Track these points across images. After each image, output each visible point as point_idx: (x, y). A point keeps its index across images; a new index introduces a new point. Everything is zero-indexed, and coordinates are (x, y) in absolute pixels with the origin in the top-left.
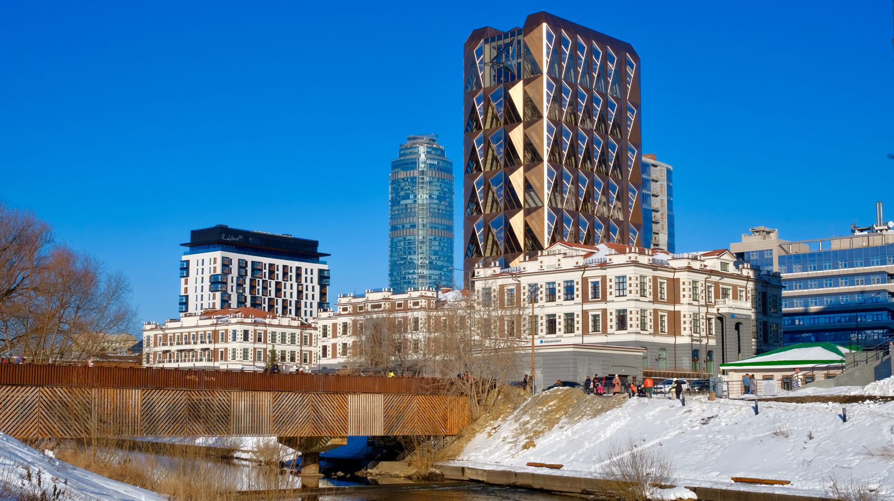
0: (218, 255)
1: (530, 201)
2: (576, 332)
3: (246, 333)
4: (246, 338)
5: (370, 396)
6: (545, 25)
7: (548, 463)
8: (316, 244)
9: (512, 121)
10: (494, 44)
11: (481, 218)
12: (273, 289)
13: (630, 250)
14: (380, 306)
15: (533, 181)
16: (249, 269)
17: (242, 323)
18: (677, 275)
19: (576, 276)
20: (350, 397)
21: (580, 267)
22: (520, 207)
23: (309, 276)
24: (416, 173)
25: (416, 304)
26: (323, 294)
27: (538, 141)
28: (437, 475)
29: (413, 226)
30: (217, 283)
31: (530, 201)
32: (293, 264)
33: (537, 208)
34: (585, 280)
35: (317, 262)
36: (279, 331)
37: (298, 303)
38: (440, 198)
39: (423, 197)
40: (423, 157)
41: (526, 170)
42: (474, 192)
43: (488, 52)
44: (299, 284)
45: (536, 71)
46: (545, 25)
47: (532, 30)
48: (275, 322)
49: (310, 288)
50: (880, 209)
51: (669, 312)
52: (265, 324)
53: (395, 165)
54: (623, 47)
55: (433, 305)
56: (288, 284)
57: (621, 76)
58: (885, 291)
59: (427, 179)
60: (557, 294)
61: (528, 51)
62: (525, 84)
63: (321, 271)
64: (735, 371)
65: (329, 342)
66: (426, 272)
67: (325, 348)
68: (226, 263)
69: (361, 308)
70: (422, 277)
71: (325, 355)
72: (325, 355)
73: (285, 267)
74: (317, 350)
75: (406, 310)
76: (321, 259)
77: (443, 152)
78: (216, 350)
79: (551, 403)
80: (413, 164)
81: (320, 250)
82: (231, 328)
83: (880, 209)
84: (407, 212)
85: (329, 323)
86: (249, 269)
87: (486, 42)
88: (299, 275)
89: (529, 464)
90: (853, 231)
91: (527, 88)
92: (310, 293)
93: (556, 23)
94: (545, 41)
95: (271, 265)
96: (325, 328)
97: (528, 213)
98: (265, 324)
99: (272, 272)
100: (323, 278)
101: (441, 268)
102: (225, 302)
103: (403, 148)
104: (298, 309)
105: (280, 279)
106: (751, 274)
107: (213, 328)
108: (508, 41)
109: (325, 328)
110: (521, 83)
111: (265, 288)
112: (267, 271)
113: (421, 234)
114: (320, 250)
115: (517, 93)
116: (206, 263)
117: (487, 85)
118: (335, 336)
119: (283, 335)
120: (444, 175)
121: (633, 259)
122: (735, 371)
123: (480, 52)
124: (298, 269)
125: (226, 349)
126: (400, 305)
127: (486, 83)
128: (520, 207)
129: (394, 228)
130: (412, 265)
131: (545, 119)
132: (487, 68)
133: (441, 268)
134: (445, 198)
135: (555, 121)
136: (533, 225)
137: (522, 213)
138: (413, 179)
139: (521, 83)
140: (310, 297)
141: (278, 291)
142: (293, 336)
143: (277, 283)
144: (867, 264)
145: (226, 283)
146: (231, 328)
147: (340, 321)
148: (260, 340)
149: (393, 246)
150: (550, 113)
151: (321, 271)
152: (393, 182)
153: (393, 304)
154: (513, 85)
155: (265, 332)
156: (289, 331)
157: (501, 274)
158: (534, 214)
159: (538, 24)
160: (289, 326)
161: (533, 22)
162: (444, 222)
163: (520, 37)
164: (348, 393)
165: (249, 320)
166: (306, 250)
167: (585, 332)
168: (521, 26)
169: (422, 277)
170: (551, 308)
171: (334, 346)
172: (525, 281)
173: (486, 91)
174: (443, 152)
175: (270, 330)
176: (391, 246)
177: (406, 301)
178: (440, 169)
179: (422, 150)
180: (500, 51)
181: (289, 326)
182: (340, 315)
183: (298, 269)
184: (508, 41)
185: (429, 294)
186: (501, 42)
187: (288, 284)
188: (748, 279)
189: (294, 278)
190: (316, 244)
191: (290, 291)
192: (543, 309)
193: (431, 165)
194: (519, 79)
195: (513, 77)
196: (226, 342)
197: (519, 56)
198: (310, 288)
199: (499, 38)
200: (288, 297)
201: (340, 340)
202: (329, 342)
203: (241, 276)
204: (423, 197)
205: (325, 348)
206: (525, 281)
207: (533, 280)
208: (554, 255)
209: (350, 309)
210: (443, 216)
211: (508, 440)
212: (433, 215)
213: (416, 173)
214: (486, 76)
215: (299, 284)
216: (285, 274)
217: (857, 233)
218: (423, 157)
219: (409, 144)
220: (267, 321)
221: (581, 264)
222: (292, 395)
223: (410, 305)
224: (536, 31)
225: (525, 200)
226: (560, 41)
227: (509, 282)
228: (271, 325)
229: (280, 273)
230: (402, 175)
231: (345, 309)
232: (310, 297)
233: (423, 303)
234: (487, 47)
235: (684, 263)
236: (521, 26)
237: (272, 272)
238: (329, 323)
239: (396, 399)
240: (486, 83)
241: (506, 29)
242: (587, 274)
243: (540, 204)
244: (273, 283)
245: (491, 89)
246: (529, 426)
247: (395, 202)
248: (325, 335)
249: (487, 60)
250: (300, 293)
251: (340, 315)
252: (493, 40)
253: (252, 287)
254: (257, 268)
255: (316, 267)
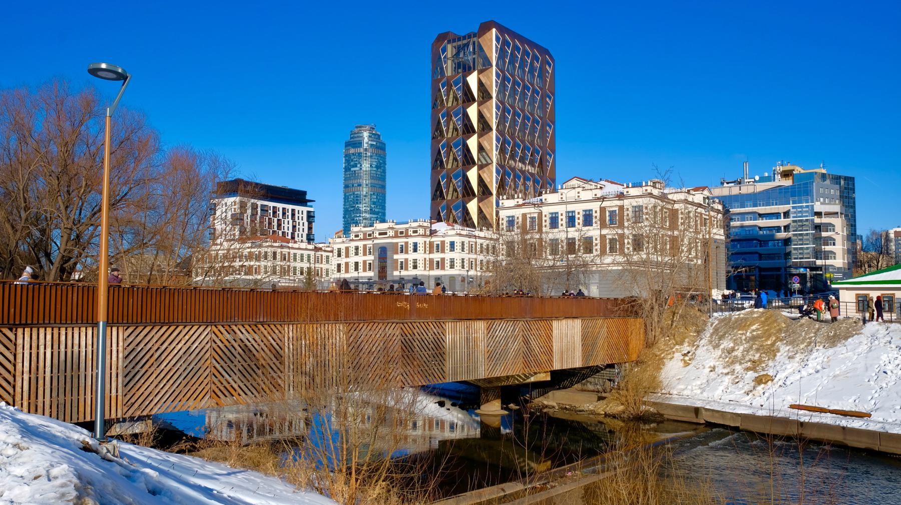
0: (237, 199)
1: (482, 159)
2: (595, 253)
3: (275, 253)
4: (275, 258)
5: (570, 321)
6: (494, 30)
7: (831, 408)
8: (304, 193)
9: (469, 101)
10: (455, 44)
11: (444, 172)
12: (275, 224)
13: (647, 183)
14: (386, 233)
15: (486, 144)
16: (259, 209)
17: (272, 246)
18: (676, 206)
19: (595, 206)
20: (555, 324)
21: (598, 198)
22: (474, 163)
23: (300, 215)
24: (362, 150)
25: (415, 232)
26: (310, 228)
27: (488, 115)
28: (653, 414)
29: (360, 185)
30: (237, 219)
31: (482, 159)
32: (290, 207)
33: (487, 164)
34: (602, 210)
35: (306, 206)
36: (299, 252)
37: (293, 234)
38: (377, 167)
39: (366, 166)
40: (366, 140)
41: (479, 137)
42: (439, 152)
43: (450, 50)
44: (294, 221)
45: (487, 64)
46: (494, 30)
47: (484, 34)
48: (296, 246)
49: (301, 224)
50: (747, 168)
51: (670, 236)
52: (289, 247)
53: (348, 145)
54: (544, 51)
55: (428, 233)
56: (286, 221)
57: (542, 71)
58: (756, 226)
59: (369, 154)
60: (577, 221)
61: (481, 48)
62: (479, 73)
63: (309, 212)
64: (847, 289)
65: (343, 260)
66: (368, 216)
67: (339, 266)
68: (243, 206)
69: (370, 235)
70: (365, 219)
71: (339, 270)
72: (339, 270)
73: (284, 209)
74: (334, 267)
75: (407, 236)
76: (309, 204)
77: (379, 136)
78: (251, 267)
79: (754, 327)
80: (359, 144)
81: (308, 198)
82: (263, 250)
83: (747, 168)
84: (356, 176)
85: (343, 247)
86: (259, 209)
87: (449, 42)
88: (293, 215)
89: (792, 407)
90: (722, 184)
91: (481, 76)
92: (301, 227)
93: (502, 30)
94: (494, 42)
95: (274, 207)
96: (339, 251)
97: (481, 167)
98: (289, 247)
99: (274, 212)
100: (310, 217)
101: (377, 213)
102: (242, 232)
103: (352, 133)
104: (293, 238)
105: (281, 217)
106: (720, 207)
107: (249, 250)
108: (465, 42)
109: (339, 251)
110: (476, 73)
111: (270, 223)
112: (271, 211)
113: (365, 190)
114: (308, 198)
115: (473, 80)
116: (229, 205)
117: (449, 74)
118: (347, 256)
119: (302, 256)
120: (380, 152)
121: (649, 191)
122: (847, 289)
123: (444, 50)
124: (293, 210)
125: (406, 260)
126: (402, 233)
127: (449, 72)
128: (474, 163)
129: (346, 187)
130: (358, 210)
131: (494, 99)
132: (449, 62)
133: (377, 213)
134: (380, 167)
135: (501, 101)
136: (485, 176)
137: (476, 168)
138: (360, 154)
139: (476, 73)
140: (301, 230)
141: (279, 225)
142: (309, 256)
143: (279, 220)
144: (743, 206)
145: (243, 220)
146: (263, 250)
147: (353, 245)
148: (285, 259)
149: (346, 198)
150: (497, 96)
151: (309, 212)
152: (346, 156)
153: (396, 232)
154: (470, 74)
155: (289, 253)
156: (306, 253)
157: (524, 204)
158: (485, 169)
159: (490, 29)
160: (306, 249)
161: (485, 28)
162: (380, 182)
163: (475, 39)
164: (551, 318)
165: (277, 244)
166: (298, 197)
167: (364, 270)
168: (476, 31)
169: (365, 219)
170: (573, 233)
171: (347, 264)
172: (546, 210)
173: (449, 79)
174: (379, 136)
175: (292, 251)
176: (344, 199)
177: (407, 230)
178: (376, 147)
179: (366, 134)
180: (459, 49)
181: (306, 249)
182: (352, 240)
183: (293, 210)
184: (465, 42)
185: (425, 224)
186: (460, 43)
187: (286, 221)
188: (718, 211)
189: (290, 217)
190: (304, 193)
191: (287, 226)
192: (561, 234)
193: (372, 145)
194: (474, 70)
195: (470, 68)
196: (407, 252)
197: (474, 53)
198: (301, 224)
199: (459, 39)
200: (286, 230)
201: (360, 259)
202: (343, 260)
203: (254, 215)
204: (366, 166)
205: (339, 266)
206: (546, 210)
207: (553, 209)
208: (574, 188)
209: (361, 236)
210: (379, 179)
211: (719, 370)
212: (372, 178)
213: (362, 150)
214: (449, 68)
215: (294, 221)
216: (284, 214)
217: (725, 185)
218: (366, 140)
219: (356, 130)
220: (290, 245)
221: (599, 196)
222: (503, 324)
223: (410, 232)
224: (488, 34)
225: (479, 159)
226: (505, 43)
227: (531, 211)
228: (293, 248)
229: (281, 213)
230: (352, 151)
231: (357, 236)
232: (301, 230)
233: (421, 231)
234: (449, 47)
235: (682, 196)
236: (476, 31)
237: (274, 212)
238: (343, 247)
239: (591, 323)
240: (449, 72)
241: (462, 33)
242: (605, 204)
243: (489, 161)
244: (276, 219)
245: (452, 77)
246: (738, 353)
247: (347, 169)
248: (339, 255)
249: (449, 56)
250: (294, 227)
251: (352, 240)
252: (454, 41)
253: (261, 222)
254: (264, 209)
255: (305, 209)
